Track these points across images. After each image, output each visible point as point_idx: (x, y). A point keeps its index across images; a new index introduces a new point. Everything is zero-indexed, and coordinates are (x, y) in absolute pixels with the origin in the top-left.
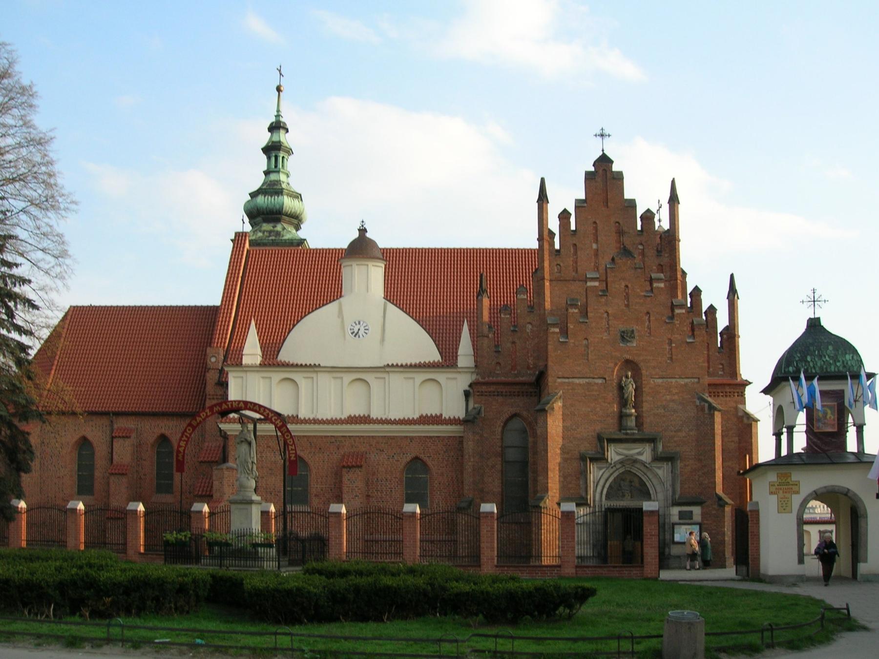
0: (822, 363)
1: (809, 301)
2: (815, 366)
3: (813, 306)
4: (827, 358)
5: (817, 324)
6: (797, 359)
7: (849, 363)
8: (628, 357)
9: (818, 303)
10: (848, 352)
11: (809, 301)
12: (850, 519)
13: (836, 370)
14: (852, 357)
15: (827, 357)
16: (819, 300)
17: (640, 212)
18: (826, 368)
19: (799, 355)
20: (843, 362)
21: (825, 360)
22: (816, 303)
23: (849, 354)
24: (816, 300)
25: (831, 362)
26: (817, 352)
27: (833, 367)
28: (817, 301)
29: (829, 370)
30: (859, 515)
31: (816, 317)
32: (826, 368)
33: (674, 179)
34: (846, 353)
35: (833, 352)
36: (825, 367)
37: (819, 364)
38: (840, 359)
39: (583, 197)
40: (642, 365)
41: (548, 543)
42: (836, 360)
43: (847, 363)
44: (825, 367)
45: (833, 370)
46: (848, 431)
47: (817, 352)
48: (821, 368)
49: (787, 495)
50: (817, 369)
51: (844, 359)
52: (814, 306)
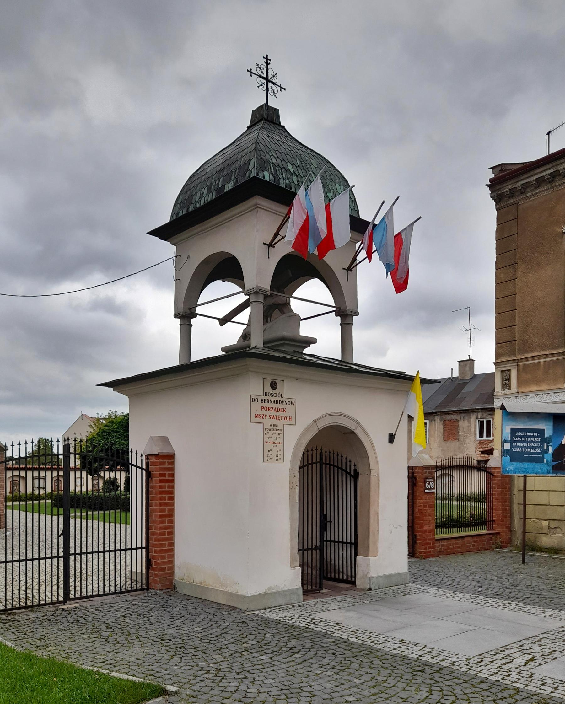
49: (280, 423)
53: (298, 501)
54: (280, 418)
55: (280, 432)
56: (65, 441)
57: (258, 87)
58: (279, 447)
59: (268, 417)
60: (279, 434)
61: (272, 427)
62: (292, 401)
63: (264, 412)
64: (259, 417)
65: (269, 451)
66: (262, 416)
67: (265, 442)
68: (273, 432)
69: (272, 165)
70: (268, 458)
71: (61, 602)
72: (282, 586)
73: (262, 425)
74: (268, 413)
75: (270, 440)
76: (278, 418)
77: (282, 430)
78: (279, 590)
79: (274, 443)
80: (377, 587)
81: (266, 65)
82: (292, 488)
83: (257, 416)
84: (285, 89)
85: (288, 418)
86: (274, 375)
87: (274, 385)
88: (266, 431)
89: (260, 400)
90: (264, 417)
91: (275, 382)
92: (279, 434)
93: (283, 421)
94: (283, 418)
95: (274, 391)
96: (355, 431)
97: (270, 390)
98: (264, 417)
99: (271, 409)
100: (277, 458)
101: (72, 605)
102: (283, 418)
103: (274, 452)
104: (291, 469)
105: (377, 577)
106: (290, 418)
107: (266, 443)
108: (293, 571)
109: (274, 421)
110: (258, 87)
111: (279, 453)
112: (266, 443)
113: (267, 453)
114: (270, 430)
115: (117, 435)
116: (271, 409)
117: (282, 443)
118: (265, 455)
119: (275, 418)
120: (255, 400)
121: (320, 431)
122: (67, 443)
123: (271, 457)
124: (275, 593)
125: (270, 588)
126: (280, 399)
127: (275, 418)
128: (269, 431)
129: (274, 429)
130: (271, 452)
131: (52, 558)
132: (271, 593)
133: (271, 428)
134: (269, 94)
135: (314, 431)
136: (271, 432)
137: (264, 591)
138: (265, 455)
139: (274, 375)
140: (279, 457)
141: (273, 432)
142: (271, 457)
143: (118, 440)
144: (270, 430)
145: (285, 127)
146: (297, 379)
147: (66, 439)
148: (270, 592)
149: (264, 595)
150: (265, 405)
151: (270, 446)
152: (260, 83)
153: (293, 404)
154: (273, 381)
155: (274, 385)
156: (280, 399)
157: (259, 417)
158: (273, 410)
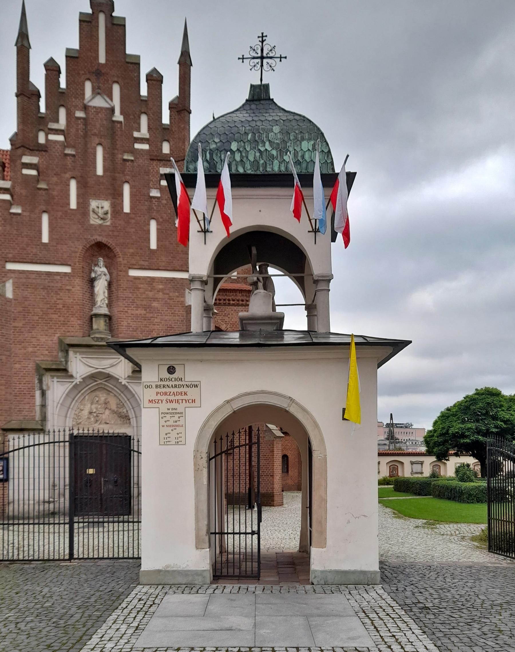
0: (258, 154)
1: (254, 58)
2: (245, 159)
3: (259, 66)
4: (268, 146)
5: (263, 96)
6: (213, 146)
7: (307, 157)
8: (99, 239)
9: (269, 61)
10: (307, 136)
11: (254, 58)
12: (299, 518)
13: (283, 169)
14: (314, 146)
15: (267, 143)
16: (271, 55)
17: (144, 71)
18: (265, 165)
19: (217, 140)
20: (296, 155)
21: (262, 149)
22: (265, 61)
23: (309, 139)
24: (265, 55)
25: (274, 152)
26: (250, 136)
27: (276, 162)
28: (268, 58)
29: (269, 169)
30: (233, 411)
31: (263, 83)
32: (265, 165)
33: (410, 342)
34: (303, 139)
35: (279, 136)
36: (262, 162)
37: (251, 158)
38: (291, 149)
39: (76, 46)
40: (117, 250)
41: (86, 547)
42: (283, 150)
43: (303, 157)
44: (262, 162)
45: (276, 169)
46: (307, 316)
47: (250, 136)
48: (255, 163)
49: (180, 407)
50: (248, 166)
51: (298, 149)
52: (262, 65)
53: (205, 482)
54: (181, 401)
55: (180, 415)
56: (70, 430)
57: (251, 70)
58: (179, 430)
59: (164, 402)
60: (179, 417)
61: (170, 411)
62: (197, 383)
63: (159, 397)
64: (154, 402)
65: (166, 434)
66: (157, 401)
67: (161, 426)
68: (171, 415)
69: (208, 153)
70: (165, 440)
71: (66, 560)
72: (184, 566)
73: (158, 409)
74: (164, 398)
75: (168, 423)
76: (178, 401)
77: (184, 413)
78: (180, 569)
79: (173, 426)
80: (322, 582)
81: (260, 44)
82: (197, 470)
83: (150, 401)
84: (286, 58)
85: (190, 401)
86: (175, 360)
87: (171, 370)
88: (163, 415)
89: (154, 386)
90: (160, 401)
91: (173, 367)
92: (179, 417)
93: (184, 404)
94: (184, 401)
95: (171, 376)
96: (287, 409)
97: (168, 376)
98: (160, 401)
99: (168, 394)
100: (177, 440)
101: (74, 563)
102: (184, 401)
103: (173, 435)
104: (196, 451)
105: (322, 572)
106: (194, 401)
107: (163, 426)
108: (198, 552)
109: (174, 405)
110: (251, 70)
111: (180, 435)
112: (163, 426)
113: (163, 435)
114: (167, 413)
115: (455, 418)
116: (168, 394)
117: (184, 426)
118: (162, 438)
119: (174, 402)
120: (148, 387)
121: (234, 412)
122: (71, 432)
123: (168, 439)
124: (174, 571)
125: (167, 566)
126: (180, 383)
127: (174, 402)
128: (166, 415)
129: (173, 412)
130: (168, 435)
131: (234, 533)
132: (168, 571)
133: (169, 411)
134: (263, 70)
135: (227, 411)
136: (168, 416)
137: (161, 568)
138: (162, 438)
139: (175, 360)
140: (180, 439)
141: (171, 415)
142: (168, 439)
143: (454, 424)
144: (167, 413)
145: (275, 100)
146: (201, 361)
147: (71, 429)
148: (168, 569)
149: (159, 571)
150: (159, 390)
151: (169, 430)
152: (253, 64)
153: (196, 386)
154: (170, 367)
155: (171, 370)
156: (180, 383)
157: (154, 402)
158: (171, 394)
